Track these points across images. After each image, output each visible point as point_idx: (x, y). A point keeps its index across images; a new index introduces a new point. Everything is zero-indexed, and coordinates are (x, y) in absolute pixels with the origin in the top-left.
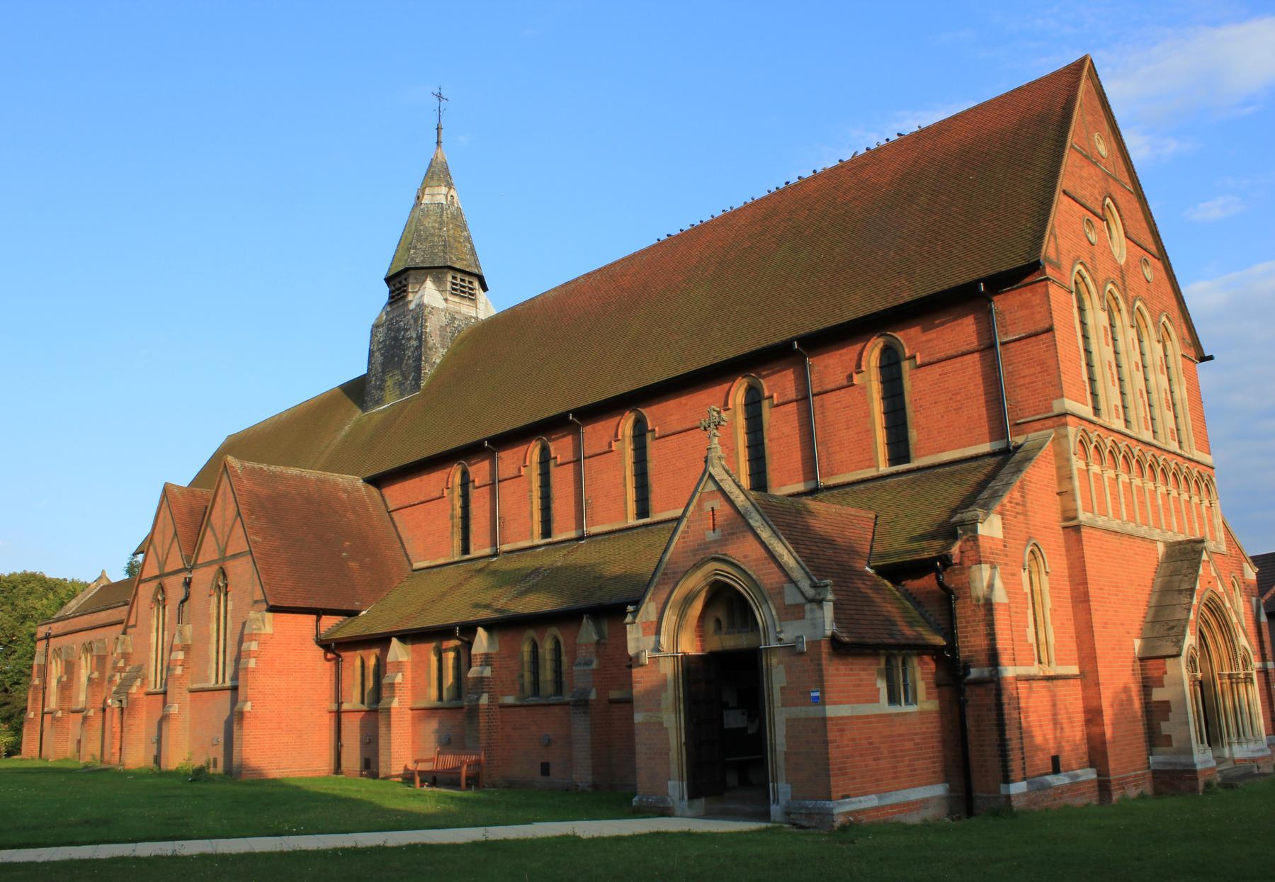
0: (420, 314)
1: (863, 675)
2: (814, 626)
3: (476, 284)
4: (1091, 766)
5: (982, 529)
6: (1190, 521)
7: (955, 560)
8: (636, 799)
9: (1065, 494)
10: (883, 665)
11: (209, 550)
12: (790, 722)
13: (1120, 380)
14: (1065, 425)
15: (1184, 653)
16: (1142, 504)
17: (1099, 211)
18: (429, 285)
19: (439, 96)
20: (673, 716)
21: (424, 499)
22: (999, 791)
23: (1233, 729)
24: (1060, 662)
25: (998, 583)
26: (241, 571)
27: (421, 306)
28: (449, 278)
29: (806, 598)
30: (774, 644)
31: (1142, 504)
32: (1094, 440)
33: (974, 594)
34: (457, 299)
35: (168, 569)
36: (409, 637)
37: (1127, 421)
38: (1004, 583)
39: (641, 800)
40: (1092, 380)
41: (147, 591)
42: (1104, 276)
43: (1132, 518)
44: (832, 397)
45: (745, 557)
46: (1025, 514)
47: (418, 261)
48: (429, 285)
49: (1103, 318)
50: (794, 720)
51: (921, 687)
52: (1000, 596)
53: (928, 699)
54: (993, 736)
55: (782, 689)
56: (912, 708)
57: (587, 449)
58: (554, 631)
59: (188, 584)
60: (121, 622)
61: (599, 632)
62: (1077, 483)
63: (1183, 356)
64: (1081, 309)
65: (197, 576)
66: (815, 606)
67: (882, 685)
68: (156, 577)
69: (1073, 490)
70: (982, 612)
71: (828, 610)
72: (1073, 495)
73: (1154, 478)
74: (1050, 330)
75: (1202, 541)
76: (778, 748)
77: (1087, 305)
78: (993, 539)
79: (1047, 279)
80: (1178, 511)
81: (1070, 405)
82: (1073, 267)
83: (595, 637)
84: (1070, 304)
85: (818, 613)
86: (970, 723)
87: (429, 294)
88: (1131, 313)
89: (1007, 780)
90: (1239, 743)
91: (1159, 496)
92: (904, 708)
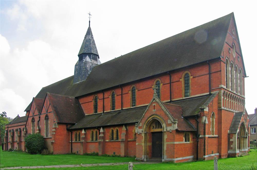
0: (86, 63)
1: (181, 136)
2: (174, 127)
3: (97, 57)
4: (218, 153)
5: (205, 110)
6: (240, 109)
7: (199, 116)
8: (136, 158)
9: (219, 103)
10: (184, 135)
11: (44, 111)
12: (167, 145)
13: (231, 81)
14: (221, 90)
15: (237, 133)
16: (232, 105)
17: (231, 46)
18: (88, 57)
19: (90, 14)
20: (144, 144)
21: (88, 102)
22: (203, 157)
23: (242, 146)
24: (215, 134)
25: (207, 120)
26: (52, 116)
27: (86, 61)
28: (92, 56)
29: (172, 122)
30: (165, 130)
31: (232, 105)
32: (226, 93)
33: (202, 122)
34: (93, 60)
35: (35, 114)
36: (104, 127)
37: (232, 89)
38: (208, 120)
39: (137, 159)
40: (227, 81)
41: (30, 119)
42: (231, 60)
43: (230, 108)
44: (175, 83)
45: (160, 114)
46: (212, 107)
47: (85, 52)
48: (88, 57)
49: (230, 69)
50: (168, 144)
51: (190, 139)
52: (207, 122)
53: (191, 141)
54: (203, 148)
55: (166, 139)
56: (189, 142)
57: (124, 92)
58: (117, 128)
59: (40, 117)
60: (25, 125)
61: (126, 128)
62: (222, 101)
63: (243, 76)
64: (226, 67)
65: (41, 116)
66: (174, 124)
67: (184, 138)
68: (32, 116)
69: (221, 102)
70: (203, 125)
71: (176, 125)
72: (221, 104)
73: (235, 100)
74: (221, 71)
75: (243, 112)
76: (165, 149)
77: (227, 66)
78: (206, 111)
79: (221, 60)
80: (238, 107)
81: (223, 86)
82: (226, 58)
83: (125, 129)
84: (224, 66)
85: (175, 125)
86: (199, 145)
87: (88, 59)
88: (235, 67)
89: (205, 155)
90: (243, 149)
91: (235, 104)
92: (187, 142)
